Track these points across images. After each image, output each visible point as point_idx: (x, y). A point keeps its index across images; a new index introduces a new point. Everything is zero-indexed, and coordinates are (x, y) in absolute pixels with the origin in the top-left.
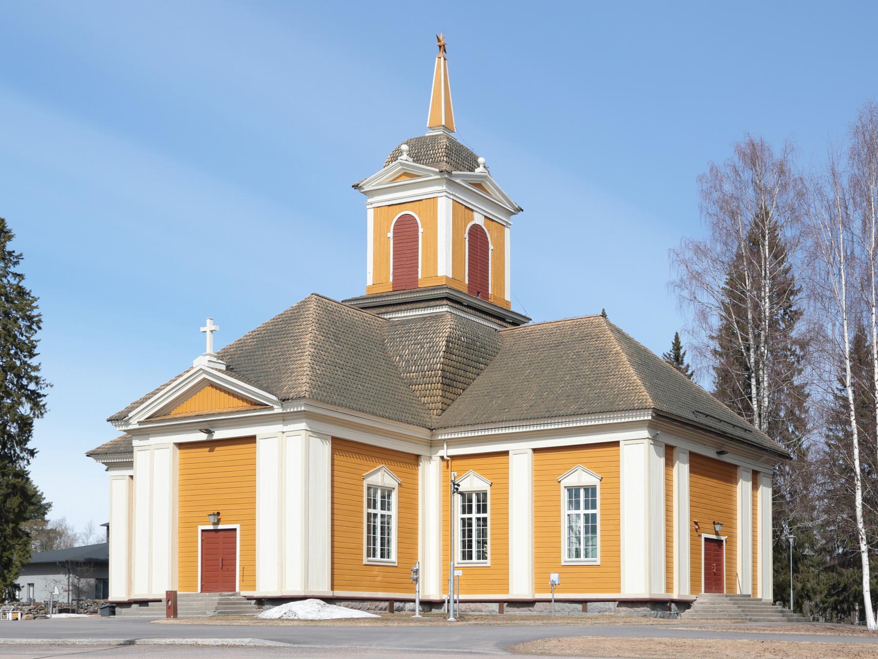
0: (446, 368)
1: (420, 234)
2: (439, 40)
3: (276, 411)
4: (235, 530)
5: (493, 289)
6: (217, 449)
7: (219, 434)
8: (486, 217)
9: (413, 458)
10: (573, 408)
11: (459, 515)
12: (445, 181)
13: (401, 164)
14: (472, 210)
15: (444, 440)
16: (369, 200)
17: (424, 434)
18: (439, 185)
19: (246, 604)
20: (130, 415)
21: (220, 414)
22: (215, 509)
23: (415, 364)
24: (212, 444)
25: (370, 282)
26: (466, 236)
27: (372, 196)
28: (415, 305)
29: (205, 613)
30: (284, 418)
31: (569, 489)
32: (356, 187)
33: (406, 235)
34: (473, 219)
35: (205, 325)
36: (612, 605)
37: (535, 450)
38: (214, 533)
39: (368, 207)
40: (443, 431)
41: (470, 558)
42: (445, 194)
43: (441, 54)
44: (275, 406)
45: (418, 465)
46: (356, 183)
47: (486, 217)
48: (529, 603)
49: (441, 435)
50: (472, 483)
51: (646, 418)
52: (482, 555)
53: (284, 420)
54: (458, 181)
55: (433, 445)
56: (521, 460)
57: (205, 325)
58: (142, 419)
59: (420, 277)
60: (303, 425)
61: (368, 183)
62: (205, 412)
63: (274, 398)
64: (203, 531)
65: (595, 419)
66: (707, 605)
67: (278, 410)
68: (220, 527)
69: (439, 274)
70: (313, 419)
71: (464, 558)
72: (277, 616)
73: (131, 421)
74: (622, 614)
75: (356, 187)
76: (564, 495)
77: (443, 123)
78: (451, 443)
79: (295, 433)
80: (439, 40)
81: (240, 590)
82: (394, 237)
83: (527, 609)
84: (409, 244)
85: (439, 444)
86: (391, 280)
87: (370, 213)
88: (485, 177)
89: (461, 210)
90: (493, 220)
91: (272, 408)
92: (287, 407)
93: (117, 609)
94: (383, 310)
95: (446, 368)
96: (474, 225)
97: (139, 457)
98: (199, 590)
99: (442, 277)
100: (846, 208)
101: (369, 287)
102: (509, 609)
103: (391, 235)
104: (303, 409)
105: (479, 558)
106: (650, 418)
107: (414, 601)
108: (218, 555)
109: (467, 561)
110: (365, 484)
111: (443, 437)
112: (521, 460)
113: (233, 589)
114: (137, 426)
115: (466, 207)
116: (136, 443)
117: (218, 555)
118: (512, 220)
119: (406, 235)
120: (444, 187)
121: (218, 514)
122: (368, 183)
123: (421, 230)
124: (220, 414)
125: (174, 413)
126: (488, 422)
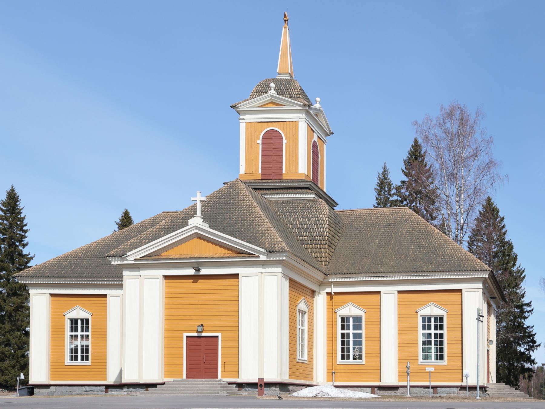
2: (285, 16)
3: (261, 259)
4: (217, 337)
6: (199, 281)
7: (204, 271)
9: (310, 292)
10: (431, 267)
11: (339, 331)
12: (305, 111)
13: (271, 96)
14: (313, 131)
15: (332, 282)
16: (242, 117)
17: (319, 276)
18: (300, 113)
19: (229, 387)
20: (128, 254)
21: (206, 258)
22: (202, 322)
23: (306, 230)
24: (195, 278)
25: (242, 171)
27: (245, 114)
28: (282, 191)
29: (218, 393)
30: (264, 264)
31: (424, 318)
32: (233, 107)
33: (272, 144)
35: (196, 197)
36: (455, 390)
37: (399, 292)
38: (196, 339)
39: (240, 121)
40: (334, 276)
41: (76, 359)
42: (304, 120)
43: (286, 26)
44: (261, 256)
45: (313, 297)
46: (234, 104)
47: (318, 137)
48: (395, 388)
49: (332, 278)
50: (350, 310)
51: (484, 276)
52: (441, 357)
53: (263, 265)
54: (311, 112)
55: (322, 284)
56: (389, 297)
57: (196, 197)
58: (138, 257)
59: (284, 172)
60: (279, 269)
61: (243, 105)
62: (208, 256)
63: (263, 250)
64: (187, 337)
65: (448, 275)
66: (496, 390)
67: (263, 258)
68: (203, 334)
70: (286, 267)
71: (72, 360)
72: (311, 395)
73: (127, 258)
74: (463, 395)
75: (233, 107)
76: (339, 321)
78: (337, 284)
79: (274, 274)
80: (285, 16)
81: (222, 377)
82: (262, 144)
83: (393, 391)
84: (275, 149)
85: (329, 284)
86: (260, 171)
88: (321, 111)
89: (311, 130)
90: (320, 139)
91: (258, 257)
92: (271, 257)
93: (36, 390)
94: (265, 192)
97: (126, 282)
98: (184, 377)
99: (302, 174)
101: (242, 175)
102: (379, 391)
103: (260, 142)
104: (284, 258)
105: (82, 360)
106: (487, 276)
107: (406, 387)
108: (202, 356)
109: (74, 362)
110: (297, 308)
111: (333, 280)
112: (389, 297)
113: (216, 377)
114: (133, 262)
115: (312, 129)
116: (125, 273)
117: (202, 356)
118: (327, 139)
119: (272, 144)
120: (304, 115)
121: (202, 325)
122: (243, 105)
123: (284, 141)
124: (206, 258)
125: (164, 255)
126: (369, 272)
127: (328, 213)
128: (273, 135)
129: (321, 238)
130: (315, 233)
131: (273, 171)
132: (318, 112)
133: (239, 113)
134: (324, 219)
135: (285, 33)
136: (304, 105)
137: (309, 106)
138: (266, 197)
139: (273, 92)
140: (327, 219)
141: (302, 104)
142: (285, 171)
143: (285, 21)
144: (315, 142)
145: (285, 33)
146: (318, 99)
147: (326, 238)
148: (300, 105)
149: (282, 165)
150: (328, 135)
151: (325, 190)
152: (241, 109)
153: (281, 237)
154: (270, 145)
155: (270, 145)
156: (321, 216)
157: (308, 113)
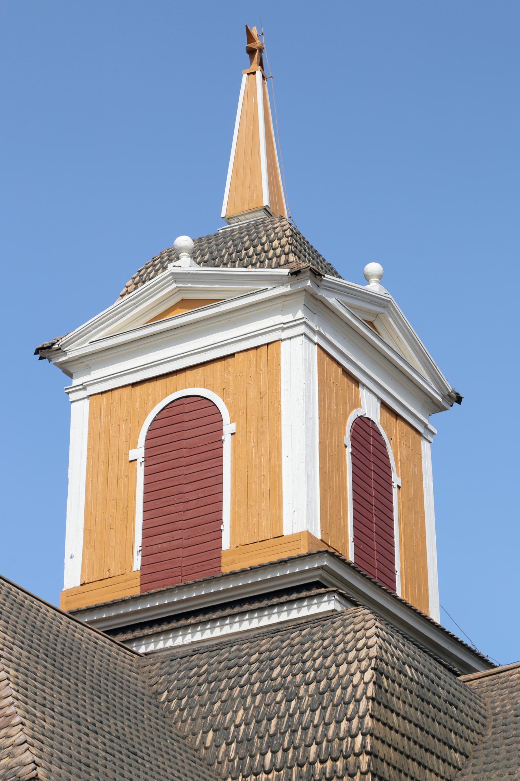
0: (382, 750)
1: (227, 439)
2: (250, 38)
5: (405, 586)
8: (384, 405)
12: (301, 299)
13: (177, 277)
14: (357, 382)
18: (283, 311)
26: (348, 441)
27: (88, 369)
32: (44, 352)
33: (184, 449)
34: (358, 404)
42: (302, 329)
46: (47, 343)
47: (384, 405)
54: (332, 300)
61: (79, 336)
69: (287, 532)
75: (44, 352)
77: (266, 202)
82: (147, 458)
86: (137, 564)
87: (80, 413)
88: (384, 304)
89: (338, 377)
90: (397, 416)
95: (382, 750)
96: (360, 418)
99: (296, 538)
100: (468, 728)
101: (72, 593)
103: (138, 453)
115: (346, 372)
119: (184, 449)
120: (300, 314)
127: (373, 652)
128: (186, 417)
129: (340, 764)
130: (313, 748)
131: (186, 552)
132: (374, 313)
133: (67, 370)
134: (356, 679)
135: (253, 91)
136: (296, 273)
137: (316, 274)
138: (142, 650)
139: (185, 264)
140: (369, 675)
141: (285, 271)
142: (232, 542)
143: (251, 52)
144: (363, 424)
145: (253, 91)
146: (374, 268)
147: (365, 759)
148: (278, 281)
149: (220, 520)
150: (441, 408)
151: (435, 616)
152: (74, 351)
153: (39, 738)
154: (173, 455)
155: (173, 455)
156: (343, 668)
157: (316, 305)
